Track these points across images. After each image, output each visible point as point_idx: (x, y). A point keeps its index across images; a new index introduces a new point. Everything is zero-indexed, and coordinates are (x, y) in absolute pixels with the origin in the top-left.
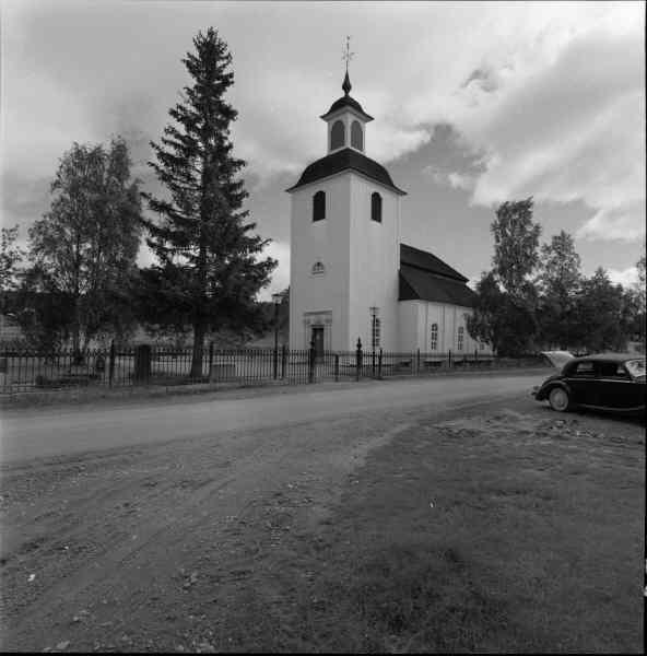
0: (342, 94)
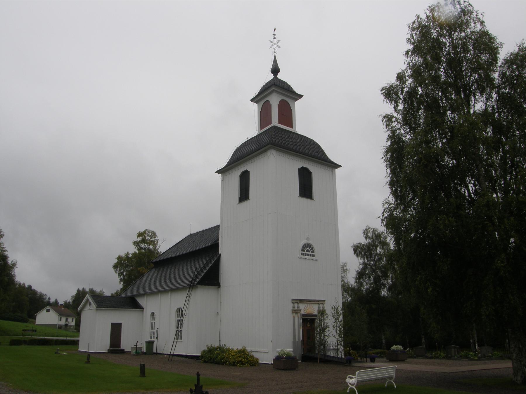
0: (271, 76)
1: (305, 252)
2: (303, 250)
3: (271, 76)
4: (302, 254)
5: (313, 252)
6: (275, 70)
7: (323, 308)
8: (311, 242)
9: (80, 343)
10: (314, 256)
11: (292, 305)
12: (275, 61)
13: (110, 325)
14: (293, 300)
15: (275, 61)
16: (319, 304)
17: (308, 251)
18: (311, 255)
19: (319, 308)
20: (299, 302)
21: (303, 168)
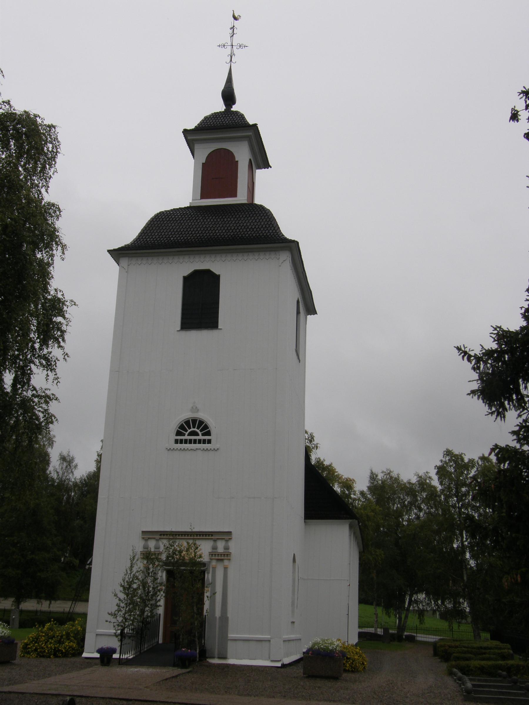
0: (221, 107)
1: (186, 437)
2: (178, 433)
3: (221, 107)
4: (176, 441)
5: (209, 433)
6: (229, 96)
7: (227, 548)
8: (201, 415)
9: (357, 626)
10: (209, 442)
11: (142, 543)
12: (229, 80)
13: (90, 600)
14: (144, 532)
15: (229, 80)
16: (215, 541)
17: (191, 434)
18: (204, 442)
19: (215, 548)
20: (158, 537)
21: (196, 273)
